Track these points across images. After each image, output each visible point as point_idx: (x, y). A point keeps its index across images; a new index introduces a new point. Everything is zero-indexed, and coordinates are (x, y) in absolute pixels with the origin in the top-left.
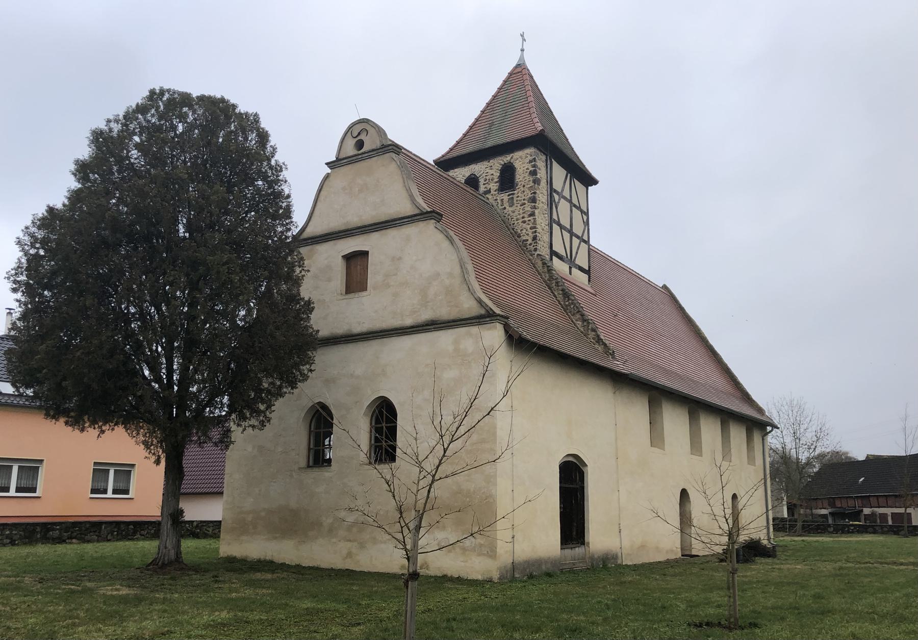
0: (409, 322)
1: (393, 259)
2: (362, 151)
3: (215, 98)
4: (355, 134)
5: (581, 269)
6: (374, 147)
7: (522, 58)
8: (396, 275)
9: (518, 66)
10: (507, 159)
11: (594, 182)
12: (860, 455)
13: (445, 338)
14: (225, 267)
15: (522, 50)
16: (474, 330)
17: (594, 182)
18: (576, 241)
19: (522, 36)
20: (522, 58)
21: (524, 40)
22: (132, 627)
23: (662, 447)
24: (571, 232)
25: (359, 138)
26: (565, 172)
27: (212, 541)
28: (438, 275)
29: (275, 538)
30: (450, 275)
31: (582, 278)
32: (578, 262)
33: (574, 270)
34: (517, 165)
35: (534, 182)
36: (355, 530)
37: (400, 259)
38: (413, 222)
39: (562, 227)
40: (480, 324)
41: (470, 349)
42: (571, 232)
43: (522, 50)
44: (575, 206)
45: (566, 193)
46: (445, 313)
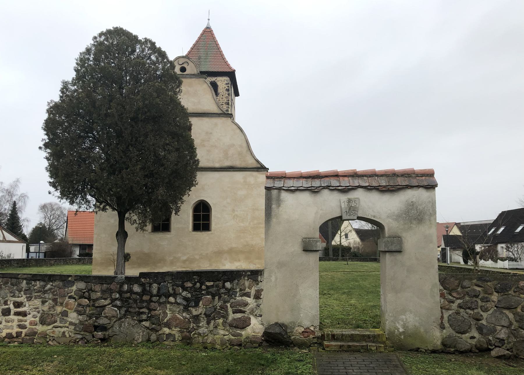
0: (217, 165)
1: (207, 133)
2: (185, 73)
4: (181, 63)
6: (193, 73)
7: (208, 24)
8: (209, 141)
10: (213, 79)
13: (239, 176)
16: (255, 173)
20: (208, 24)
25: (183, 65)
27: (374, 265)
28: (234, 145)
29: (134, 267)
30: (241, 146)
34: (219, 83)
35: (229, 95)
36: (187, 262)
37: (211, 133)
38: (219, 116)
40: (257, 171)
41: (252, 182)
46: (238, 163)
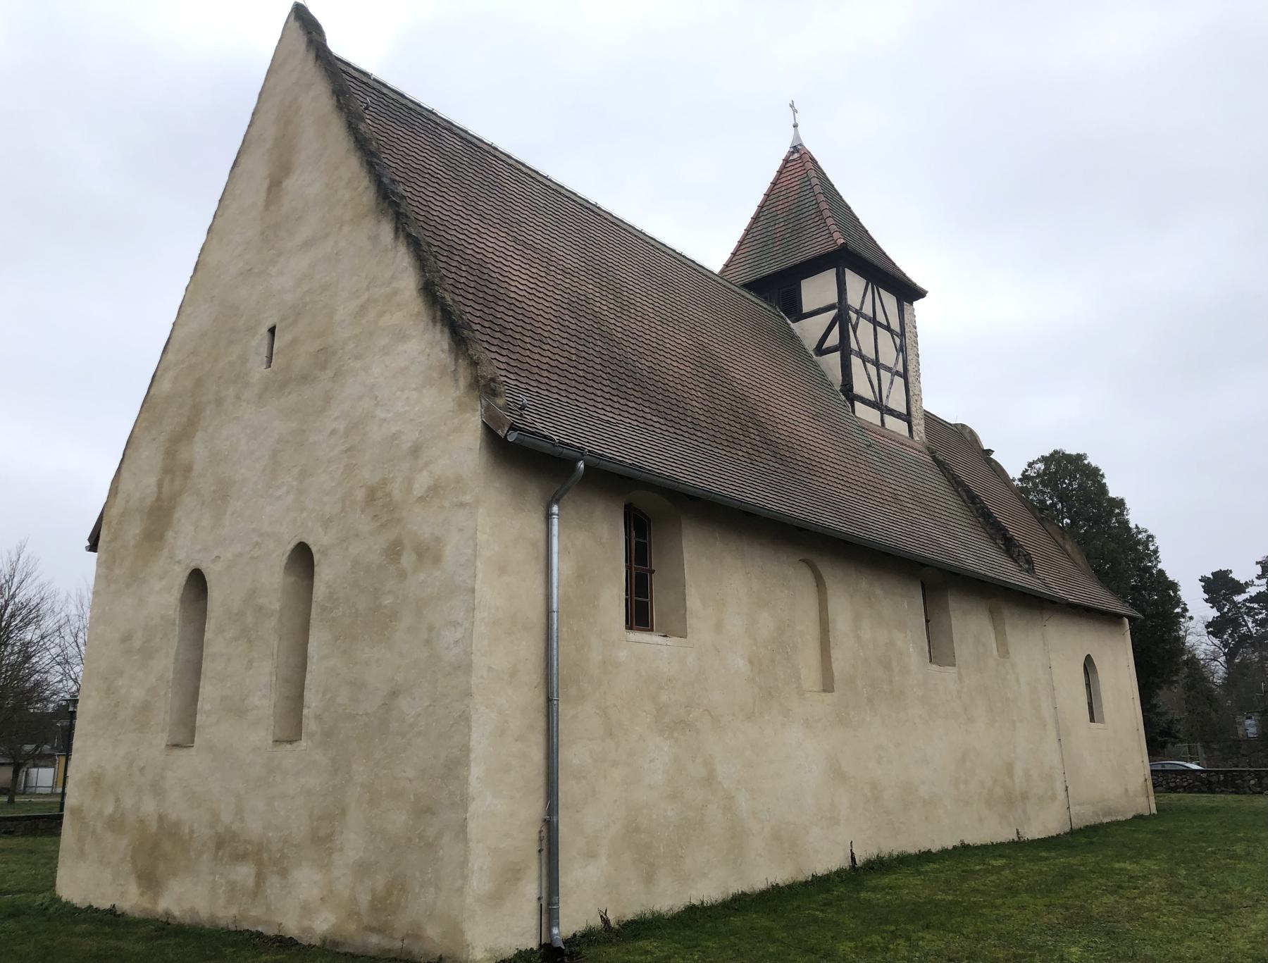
3: (203, 928)
5: (898, 415)
7: (797, 136)
9: (795, 149)
11: (919, 294)
12: (952, 420)
14: (384, 520)
15: (795, 126)
17: (919, 294)
18: (886, 376)
19: (792, 106)
20: (797, 136)
21: (795, 111)
22: (264, 958)
23: (1102, 721)
24: (877, 363)
26: (864, 282)
31: (896, 426)
32: (892, 405)
33: (888, 418)
39: (864, 359)
42: (877, 363)
43: (795, 126)
44: (881, 325)
45: (867, 310)
